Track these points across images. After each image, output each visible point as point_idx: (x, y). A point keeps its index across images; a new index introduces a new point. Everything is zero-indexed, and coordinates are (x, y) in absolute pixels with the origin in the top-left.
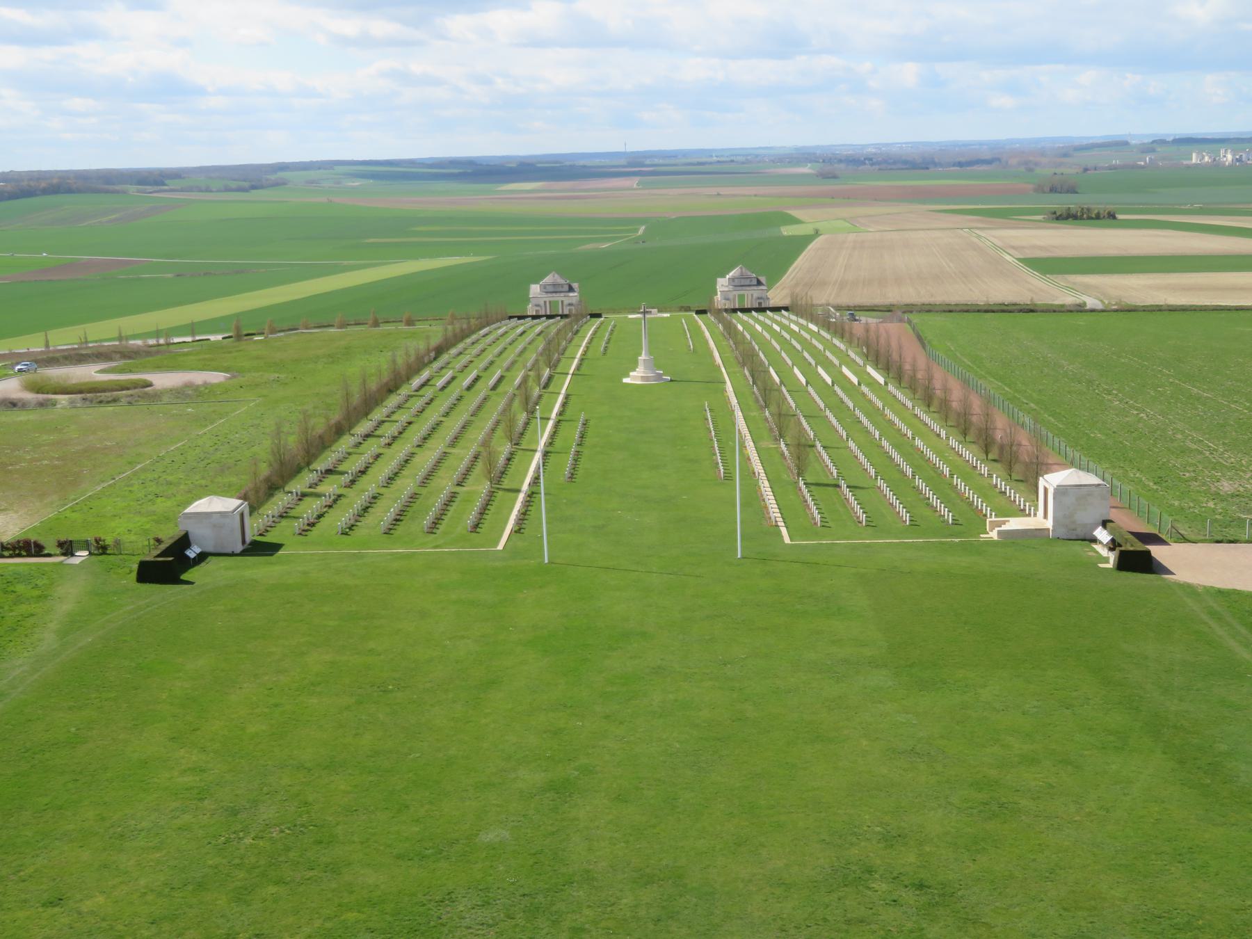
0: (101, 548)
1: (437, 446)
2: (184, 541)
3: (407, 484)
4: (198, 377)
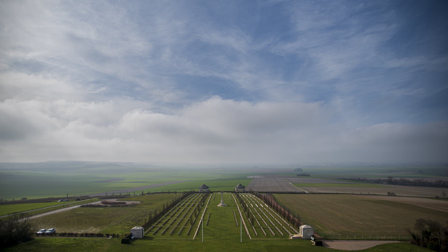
0: (114, 236)
1: (181, 218)
2: (131, 235)
3: (175, 225)
4: (135, 202)
